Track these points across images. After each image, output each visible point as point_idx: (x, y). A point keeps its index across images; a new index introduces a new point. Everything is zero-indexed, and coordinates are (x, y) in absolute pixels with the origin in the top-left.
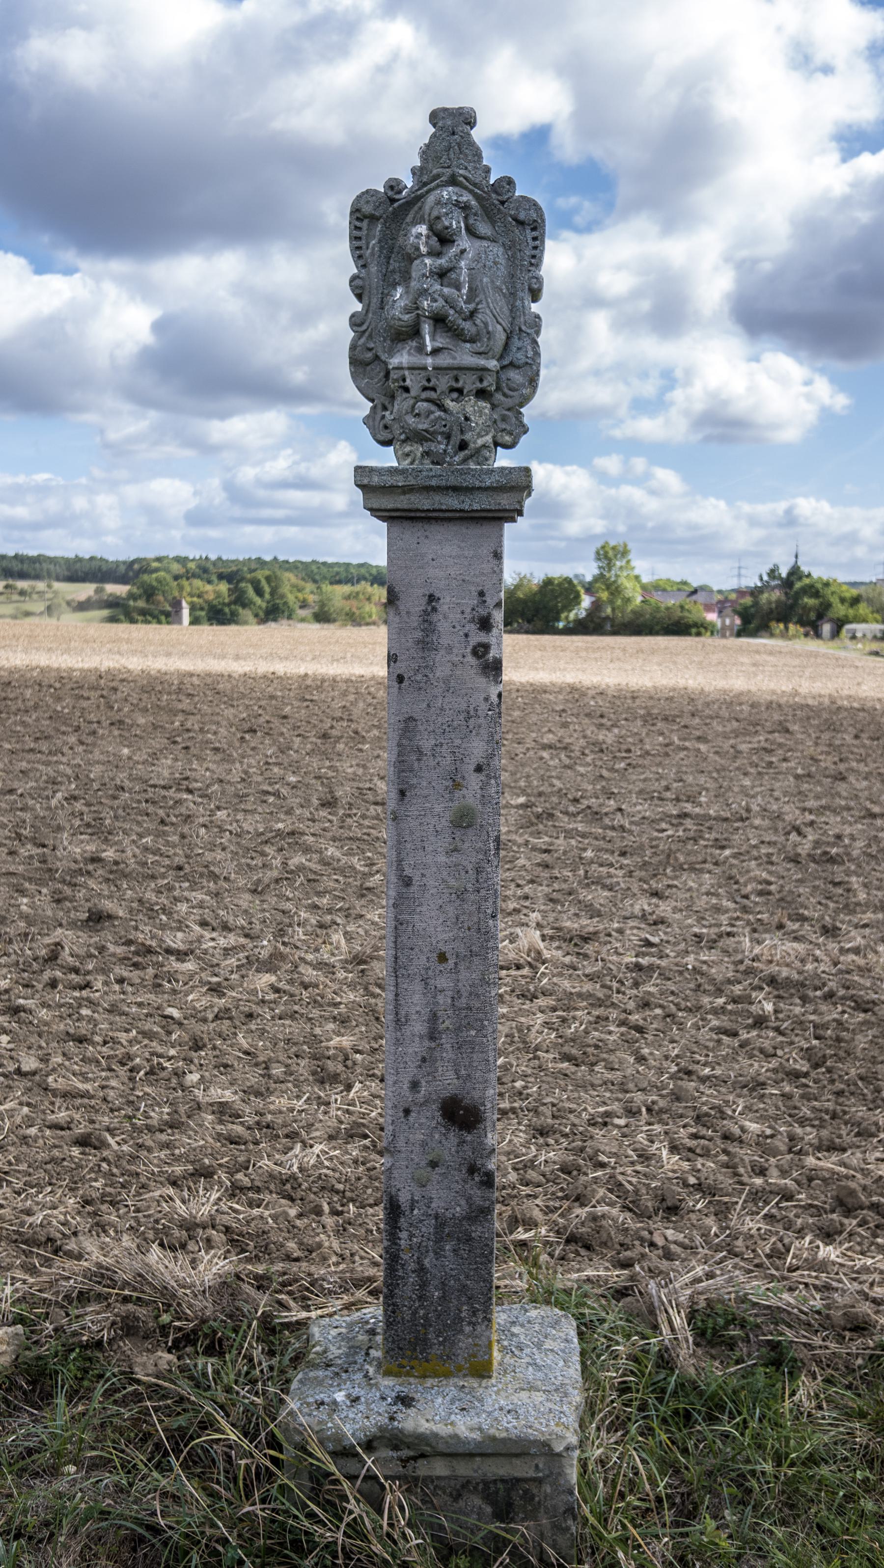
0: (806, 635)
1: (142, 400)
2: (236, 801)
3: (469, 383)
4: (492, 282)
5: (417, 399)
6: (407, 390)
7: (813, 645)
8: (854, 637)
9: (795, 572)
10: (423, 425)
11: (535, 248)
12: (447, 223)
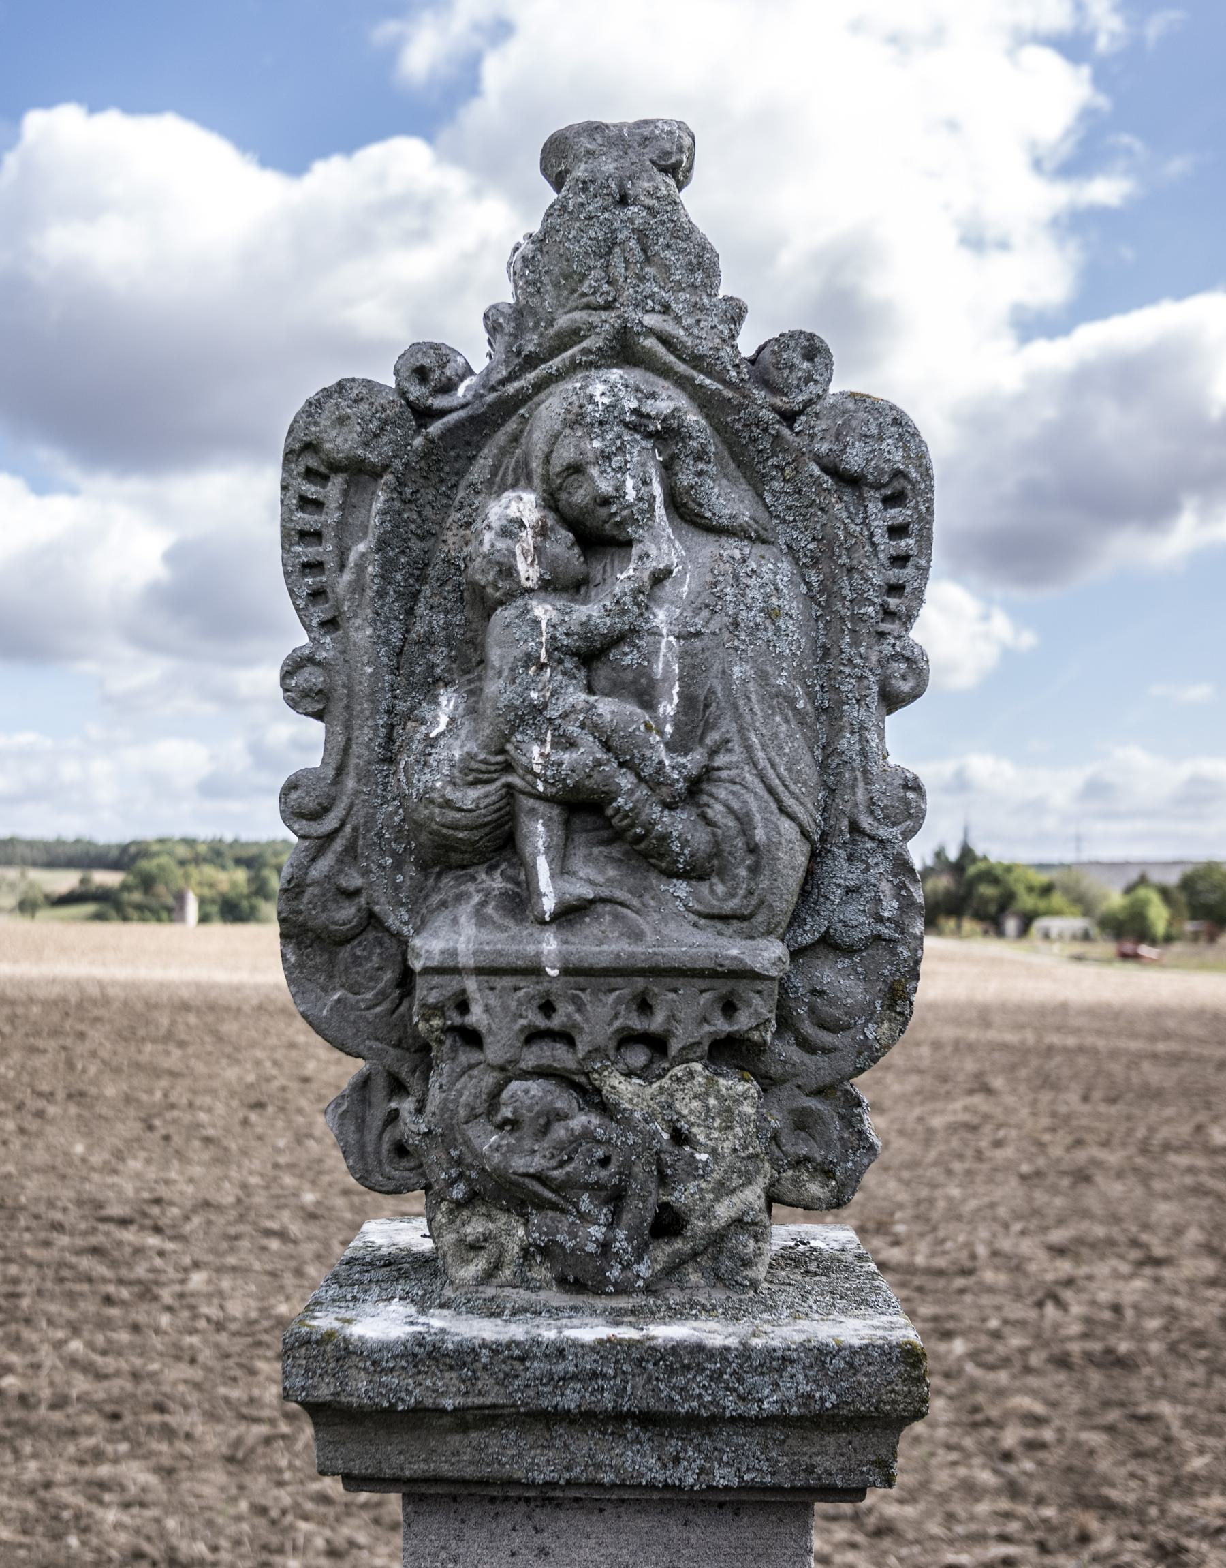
0: (986, 933)
1: (148, 644)
2: (225, 1245)
3: (686, 1016)
4: (763, 676)
5: (508, 1072)
6: (473, 1038)
7: (993, 948)
8: (1046, 936)
9: (967, 853)
10: (528, 1161)
11: (900, 560)
12: (605, 487)
